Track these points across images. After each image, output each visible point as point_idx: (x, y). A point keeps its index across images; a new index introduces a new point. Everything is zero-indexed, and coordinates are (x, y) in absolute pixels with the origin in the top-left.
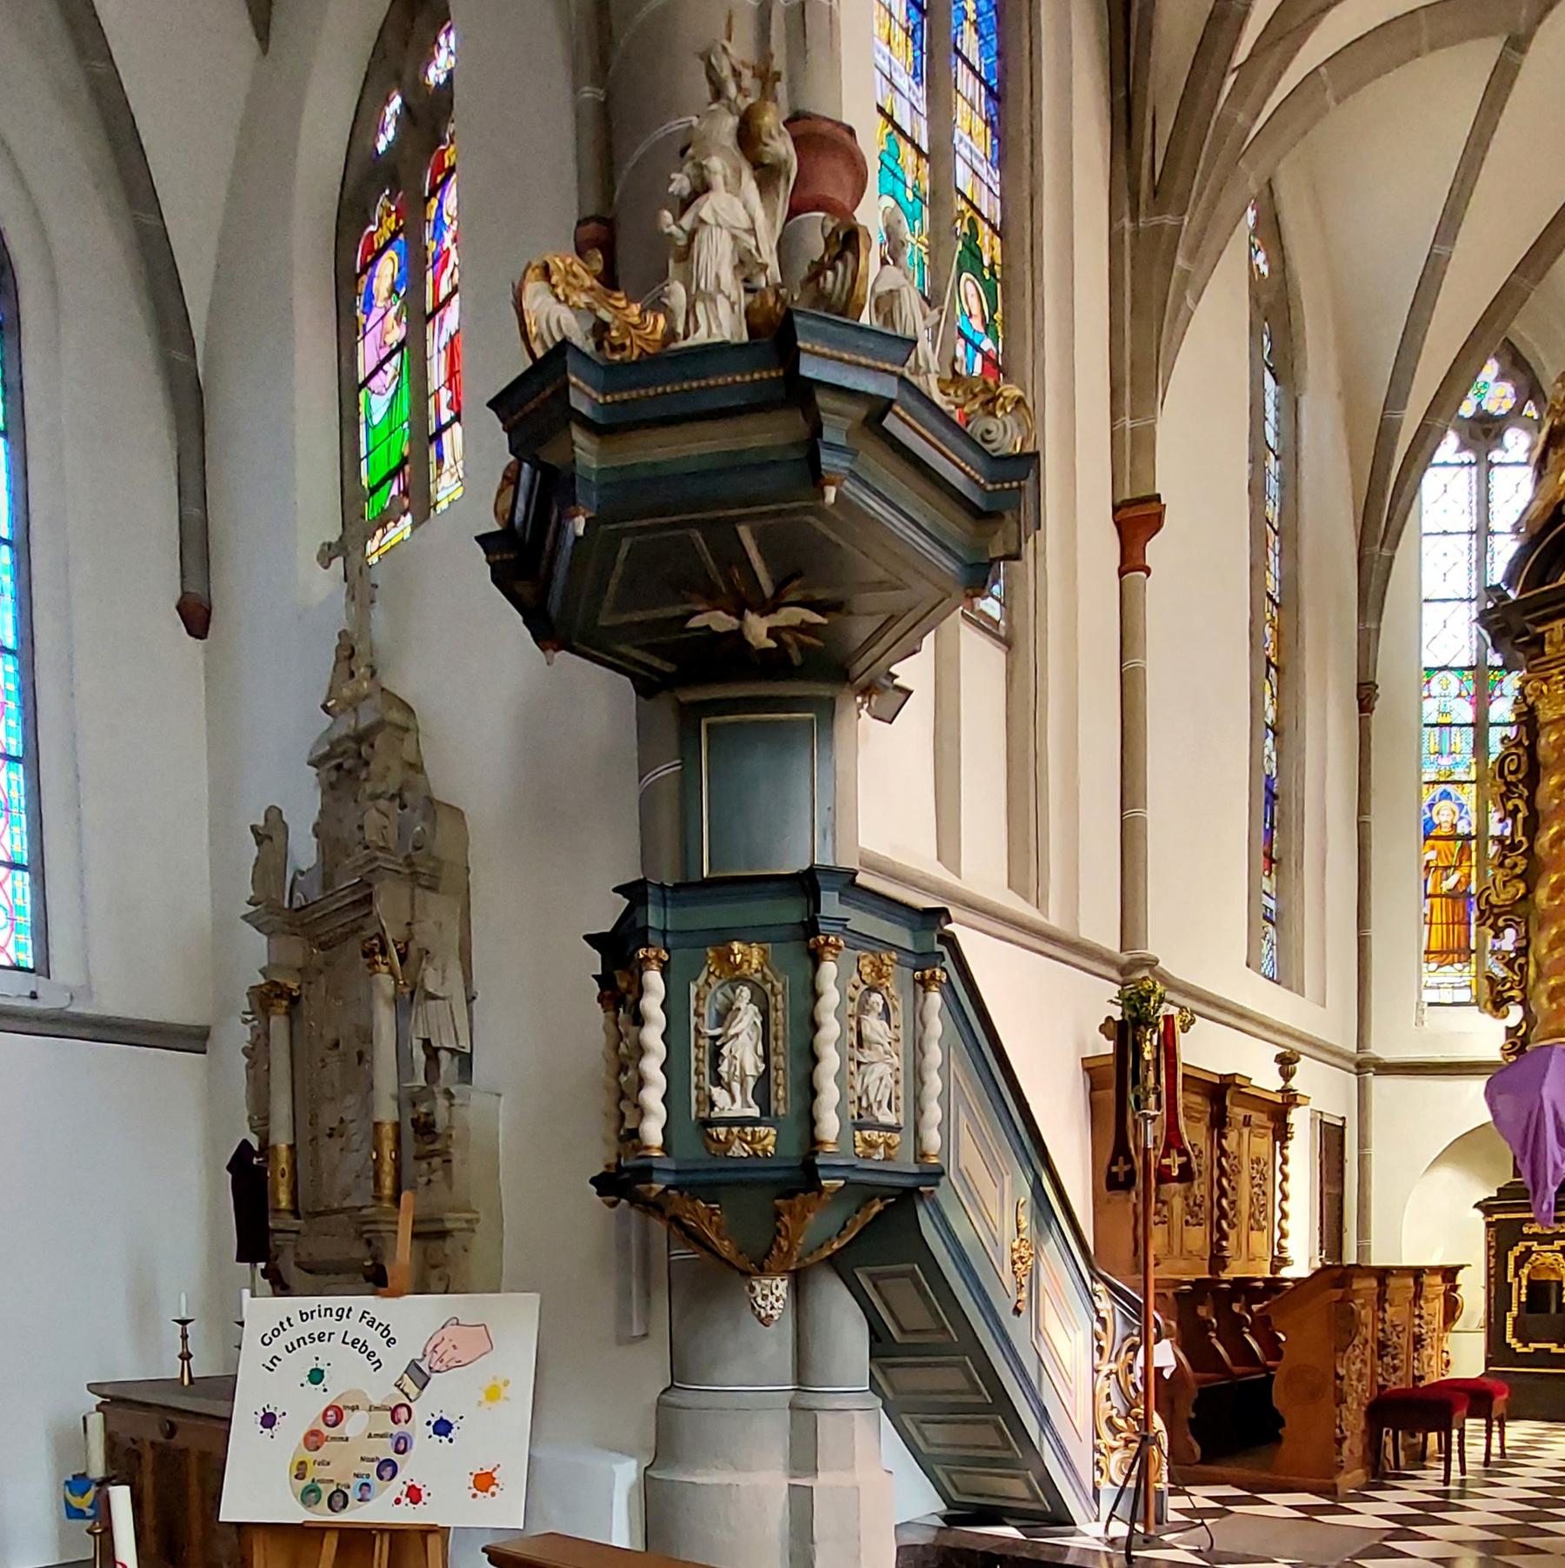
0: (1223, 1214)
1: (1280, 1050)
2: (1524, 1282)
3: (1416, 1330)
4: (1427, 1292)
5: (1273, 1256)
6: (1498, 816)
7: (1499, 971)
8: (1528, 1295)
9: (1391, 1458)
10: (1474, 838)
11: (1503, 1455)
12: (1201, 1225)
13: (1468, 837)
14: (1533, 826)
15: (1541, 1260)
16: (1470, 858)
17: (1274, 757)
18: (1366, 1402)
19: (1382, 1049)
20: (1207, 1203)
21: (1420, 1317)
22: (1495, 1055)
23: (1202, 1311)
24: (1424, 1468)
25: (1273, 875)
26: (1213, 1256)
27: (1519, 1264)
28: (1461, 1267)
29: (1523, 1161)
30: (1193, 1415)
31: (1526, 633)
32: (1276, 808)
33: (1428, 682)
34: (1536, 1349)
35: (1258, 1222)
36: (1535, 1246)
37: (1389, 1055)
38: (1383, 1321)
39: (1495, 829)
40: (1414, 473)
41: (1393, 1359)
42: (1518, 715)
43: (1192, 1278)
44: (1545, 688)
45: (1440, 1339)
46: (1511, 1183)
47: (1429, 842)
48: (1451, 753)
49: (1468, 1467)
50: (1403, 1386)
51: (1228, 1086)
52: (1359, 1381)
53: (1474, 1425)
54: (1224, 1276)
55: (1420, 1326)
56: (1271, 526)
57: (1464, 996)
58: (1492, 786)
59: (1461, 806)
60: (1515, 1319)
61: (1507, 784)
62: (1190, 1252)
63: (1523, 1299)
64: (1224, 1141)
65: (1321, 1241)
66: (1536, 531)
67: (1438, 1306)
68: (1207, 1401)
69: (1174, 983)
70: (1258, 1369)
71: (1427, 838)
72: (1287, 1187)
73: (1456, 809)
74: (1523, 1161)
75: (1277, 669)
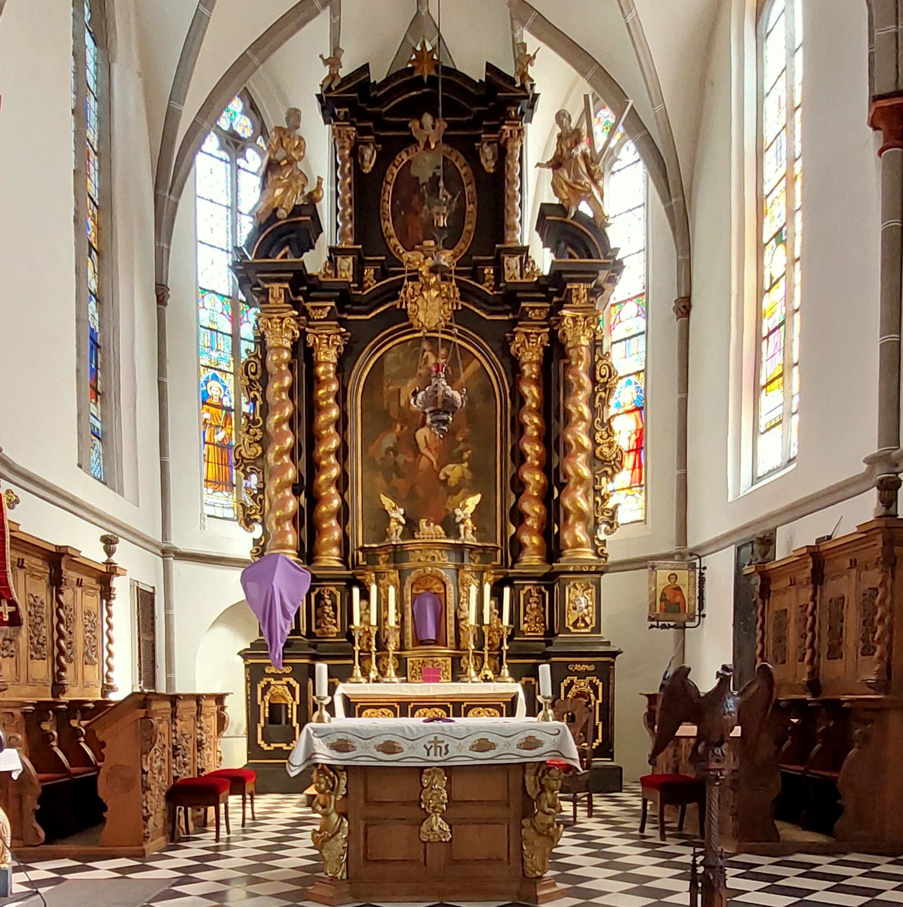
0: (62, 652)
1: (105, 533)
2: (267, 705)
3: (199, 737)
4: (204, 710)
5: (103, 684)
6: (246, 400)
7: (250, 503)
8: (270, 713)
9: (184, 827)
10: (232, 410)
11: (254, 818)
12: (44, 659)
13: (229, 409)
14: (265, 410)
15: (276, 690)
16: (231, 424)
17: (96, 316)
18: (165, 789)
19: (179, 542)
20: (49, 643)
21: (201, 728)
22: (248, 556)
23: (46, 726)
24: (206, 831)
25: (99, 403)
26: (54, 683)
27: (264, 693)
28: (227, 694)
29: (264, 626)
30: (38, 807)
31: (259, 286)
32: (99, 355)
33: (203, 297)
34: (275, 748)
35: (90, 658)
36: (273, 681)
37: (184, 548)
38: (175, 731)
39: (246, 408)
40: (189, 152)
41: (184, 757)
42: (256, 337)
43: (34, 700)
44: (270, 325)
45: (215, 743)
46: (259, 640)
47: (206, 407)
48: (218, 350)
49: (232, 828)
50: (191, 776)
51: (63, 555)
52: (160, 774)
53: (234, 800)
54: (64, 698)
55: (201, 734)
56: (92, 147)
57: (230, 514)
58: (241, 379)
59: (225, 387)
60: (262, 729)
61: (250, 380)
62: (35, 680)
63: (267, 715)
64: (61, 596)
65: (140, 674)
66: (263, 220)
67: (214, 720)
68: (48, 795)
69: (16, 468)
70: (91, 769)
71: (204, 403)
72: (113, 634)
73: (222, 389)
74: (264, 626)
75: (97, 254)
